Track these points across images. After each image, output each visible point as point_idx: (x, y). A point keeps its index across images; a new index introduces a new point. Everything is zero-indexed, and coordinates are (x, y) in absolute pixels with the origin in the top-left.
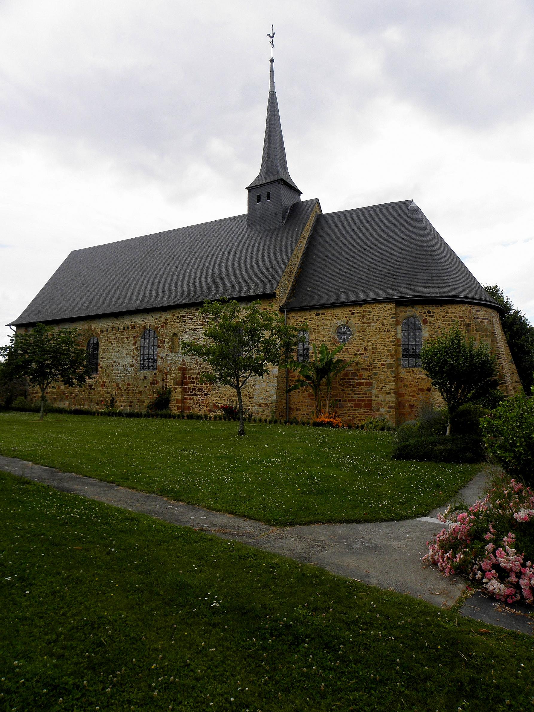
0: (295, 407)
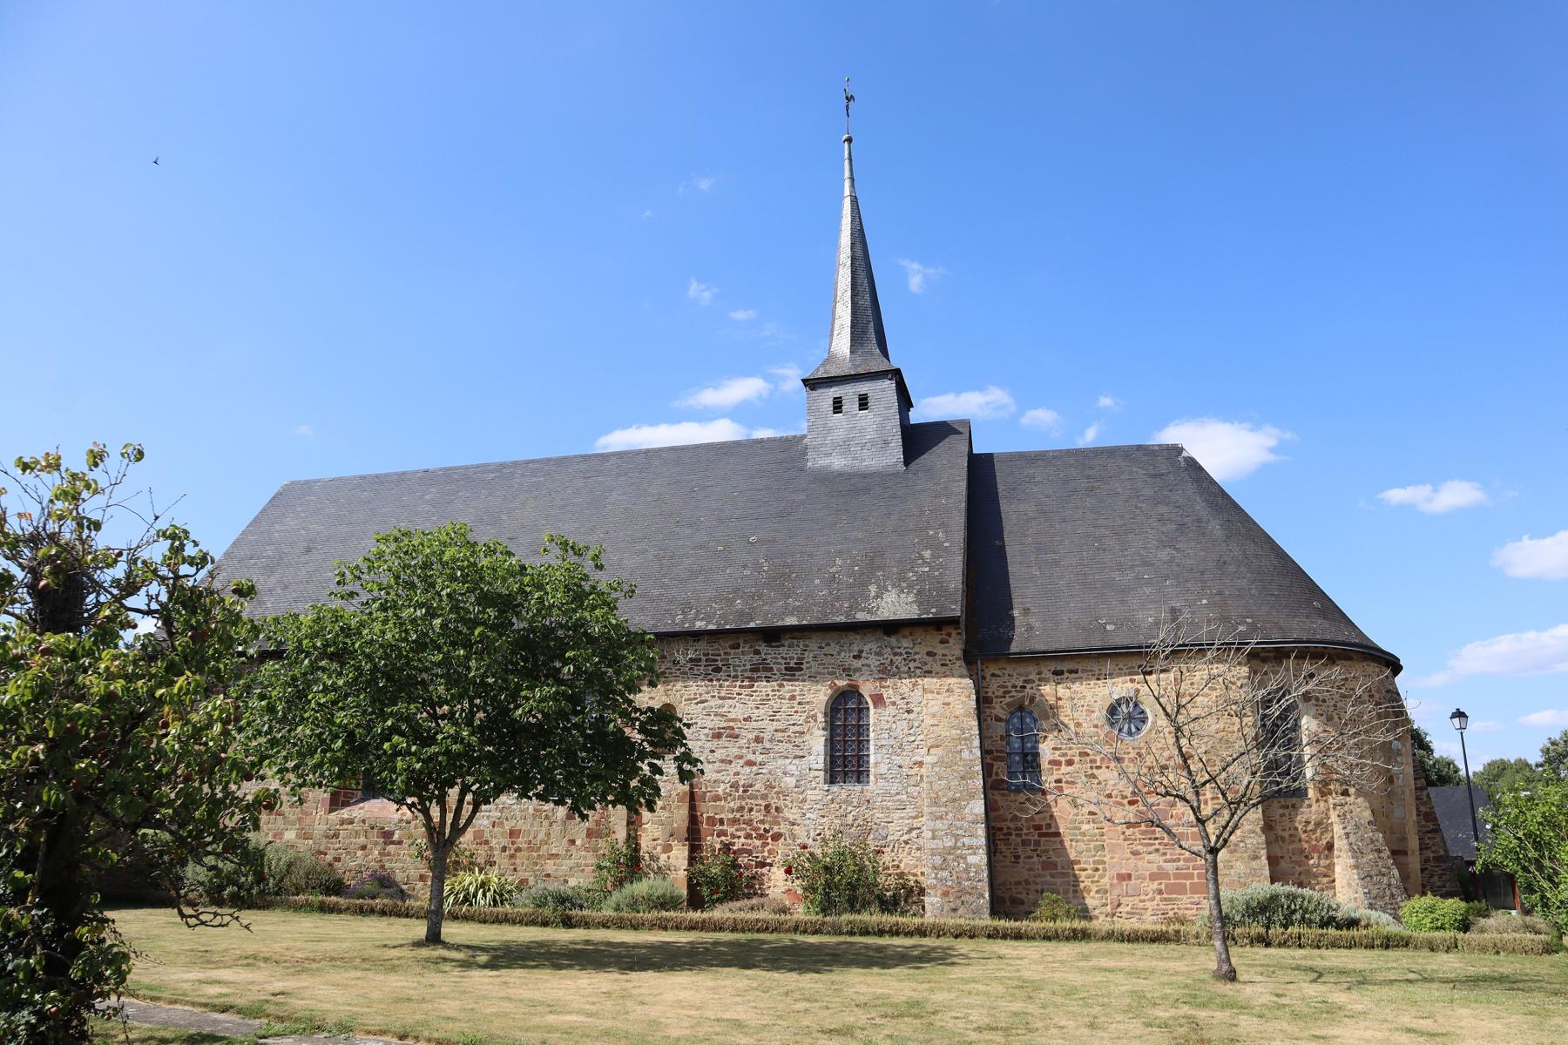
0: (1007, 896)
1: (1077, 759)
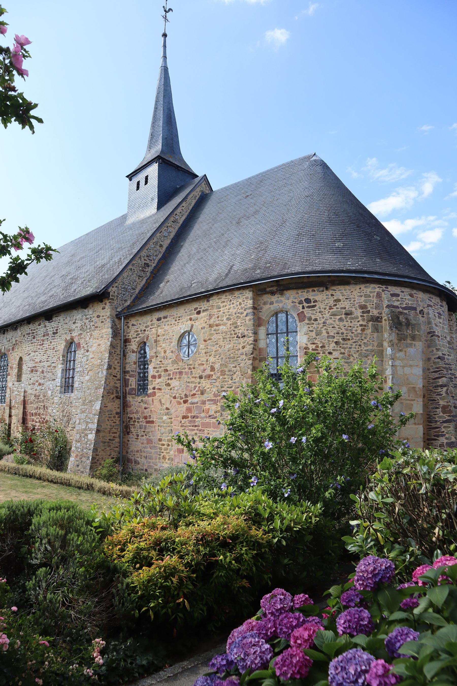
0: (133, 458)
1: (163, 373)
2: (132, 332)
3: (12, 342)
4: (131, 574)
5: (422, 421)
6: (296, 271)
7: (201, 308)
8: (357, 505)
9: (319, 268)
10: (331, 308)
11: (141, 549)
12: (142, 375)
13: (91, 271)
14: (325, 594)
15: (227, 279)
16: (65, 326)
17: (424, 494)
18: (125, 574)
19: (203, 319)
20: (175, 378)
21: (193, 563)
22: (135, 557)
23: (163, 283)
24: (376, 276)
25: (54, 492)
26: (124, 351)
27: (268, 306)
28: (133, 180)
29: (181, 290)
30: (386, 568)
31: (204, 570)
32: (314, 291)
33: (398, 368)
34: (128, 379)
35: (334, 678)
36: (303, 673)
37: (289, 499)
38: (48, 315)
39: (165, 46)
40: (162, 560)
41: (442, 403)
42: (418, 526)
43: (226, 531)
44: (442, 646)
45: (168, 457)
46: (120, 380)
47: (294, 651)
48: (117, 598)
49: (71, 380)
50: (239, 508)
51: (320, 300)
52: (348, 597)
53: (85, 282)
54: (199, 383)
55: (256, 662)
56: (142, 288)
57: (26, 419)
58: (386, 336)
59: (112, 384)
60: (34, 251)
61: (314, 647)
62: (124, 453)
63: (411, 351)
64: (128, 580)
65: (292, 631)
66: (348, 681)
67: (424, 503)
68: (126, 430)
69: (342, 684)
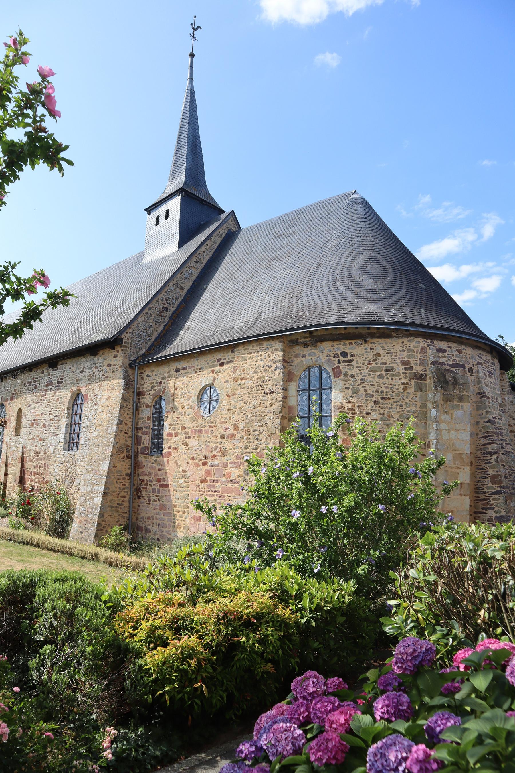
0: (144, 526)
1: (180, 431)
2: (147, 384)
3: (10, 392)
4: (145, 655)
5: (468, 492)
6: (332, 321)
7: (224, 359)
8: (397, 584)
9: (358, 319)
10: (370, 363)
11: (157, 628)
12: (156, 432)
13: (102, 314)
14: (361, 677)
15: (255, 328)
16: (72, 375)
17: (470, 572)
18: (139, 655)
19: (227, 372)
20: (194, 437)
21: (213, 643)
22: (149, 636)
23: (183, 330)
24: (421, 329)
25: (54, 561)
26: (137, 405)
27: (299, 359)
28: (152, 214)
29: (203, 338)
30: (426, 650)
31: (226, 652)
32: (352, 344)
33: (443, 432)
34: (141, 437)
35: (373, 765)
36: (339, 758)
37: (319, 576)
38: (53, 362)
39: (192, 67)
40: (179, 640)
41: (491, 472)
42: (462, 607)
43: (250, 610)
44: (486, 731)
45: (183, 526)
46: (132, 437)
47: (329, 736)
48: (128, 681)
49: (76, 435)
50: (264, 584)
51: (358, 354)
52: (385, 681)
53: (95, 326)
54: (221, 443)
55: (288, 748)
56: (159, 335)
57: (24, 479)
58: (430, 396)
59: (123, 441)
60: (50, 296)
61: (350, 731)
62: (134, 520)
63: (458, 413)
64: (141, 661)
65: (327, 716)
66: (388, 768)
67: (469, 582)
68: (137, 494)
69: (381, 771)
